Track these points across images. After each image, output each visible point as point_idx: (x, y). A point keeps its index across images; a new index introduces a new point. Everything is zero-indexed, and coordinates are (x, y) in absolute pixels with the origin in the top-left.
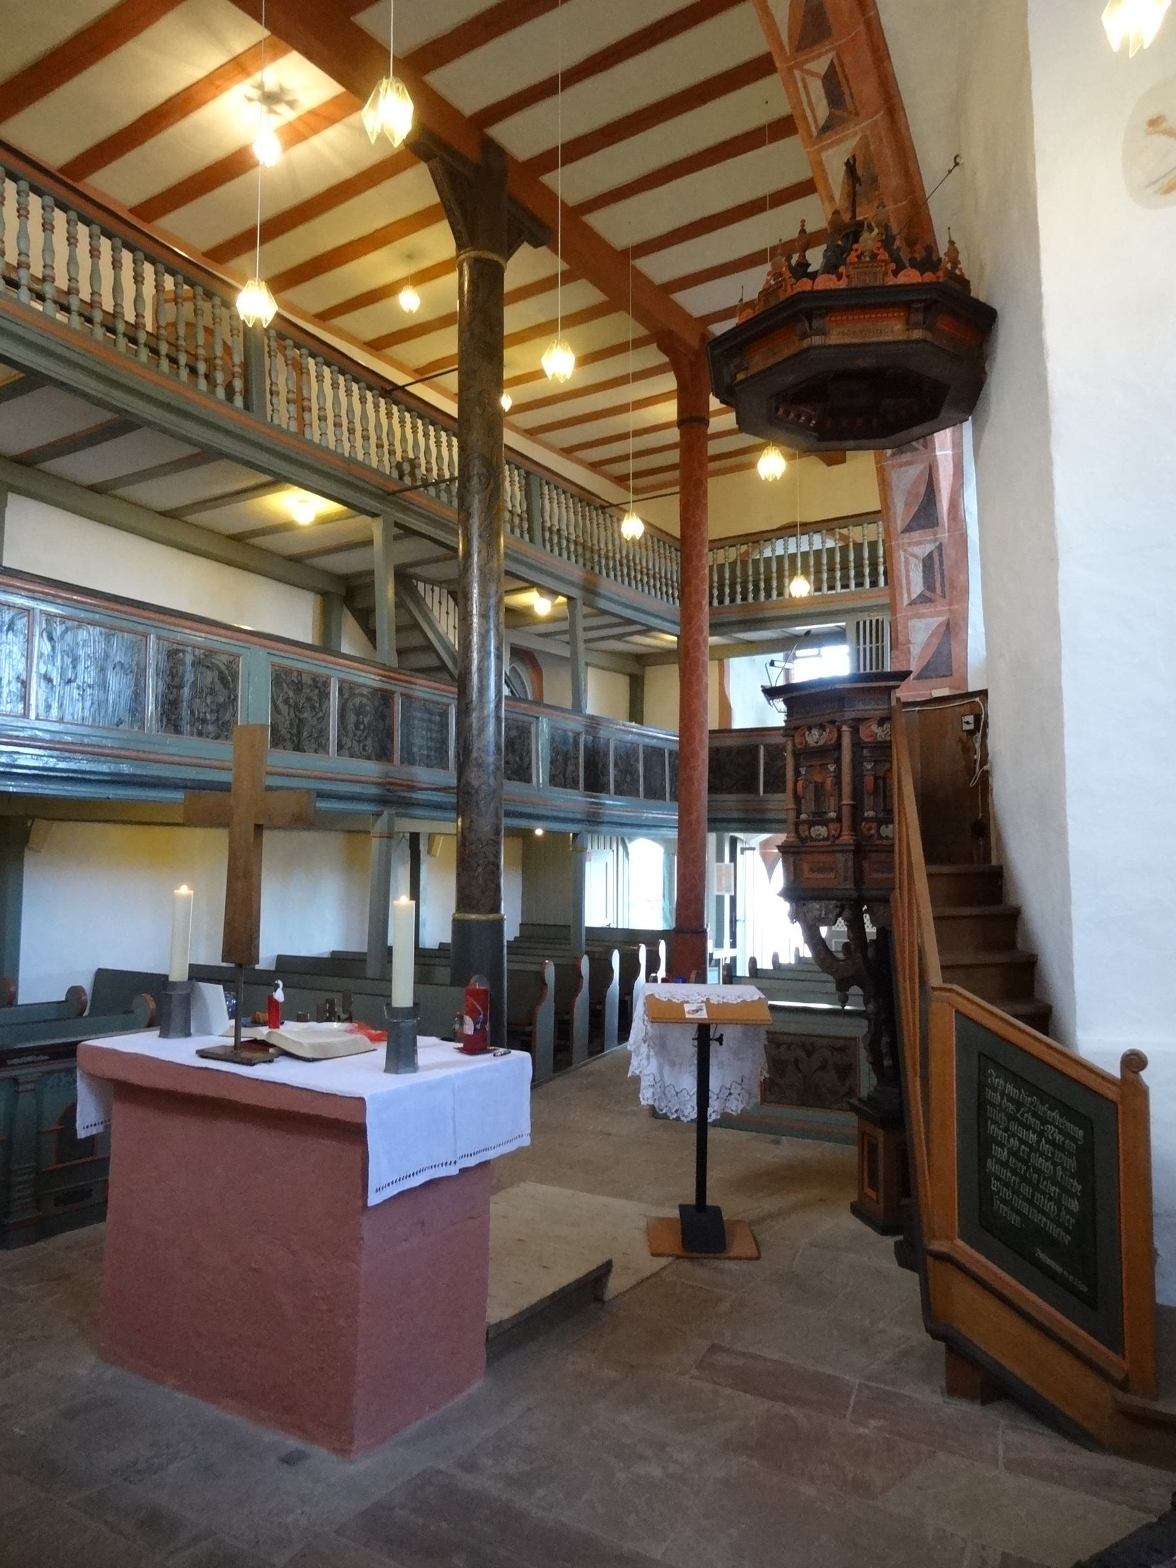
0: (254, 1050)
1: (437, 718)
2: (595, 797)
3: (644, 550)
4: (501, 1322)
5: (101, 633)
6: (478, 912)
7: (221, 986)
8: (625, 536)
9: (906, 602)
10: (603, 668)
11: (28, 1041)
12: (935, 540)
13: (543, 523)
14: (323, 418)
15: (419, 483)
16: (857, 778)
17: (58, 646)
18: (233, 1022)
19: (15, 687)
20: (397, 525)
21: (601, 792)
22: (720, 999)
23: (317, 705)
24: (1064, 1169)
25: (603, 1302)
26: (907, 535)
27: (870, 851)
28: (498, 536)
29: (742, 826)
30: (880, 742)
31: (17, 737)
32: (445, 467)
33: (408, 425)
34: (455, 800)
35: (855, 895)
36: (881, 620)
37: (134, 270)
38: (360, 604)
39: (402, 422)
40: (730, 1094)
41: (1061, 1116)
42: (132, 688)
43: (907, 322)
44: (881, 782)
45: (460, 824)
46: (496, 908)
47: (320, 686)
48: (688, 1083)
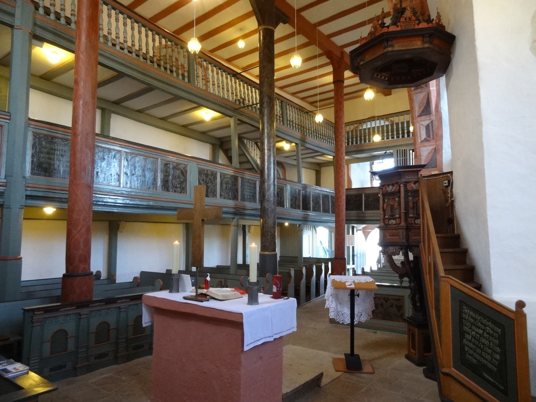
0: (201, 297)
1: (253, 185)
2: (306, 212)
3: (321, 127)
4: (287, 393)
5: (143, 158)
6: (268, 251)
7: (189, 275)
8: (316, 122)
9: (419, 141)
10: (308, 168)
11: (122, 294)
12: (430, 119)
13: (287, 118)
14: (213, 85)
15: (245, 106)
16: (407, 203)
17: (130, 163)
18: (194, 288)
19: (116, 177)
20: (239, 120)
21: (308, 210)
22: (358, 281)
23: (213, 181)
24: (493, 343)
25: (320, 387)
26: (419, 118)
27: (411, 229)
28: (273, 122)
29: (356, 222)
30: (414, 190)
31: (117, 193)
32: (254, 100)
33: (242, 86)
34: (260, 214)
35: (407, 244)
36: (406, 149)
37: (152, 37)
38: (225, 147)
39: (240, 85)
40: (361, 315)
41: (492, 324)
42: (153, 177)
43: (423, 41)
44: (415, 204)
45: (261, 221)
46: (274, 250)
47: (214, 175)
48: (347, 311)
